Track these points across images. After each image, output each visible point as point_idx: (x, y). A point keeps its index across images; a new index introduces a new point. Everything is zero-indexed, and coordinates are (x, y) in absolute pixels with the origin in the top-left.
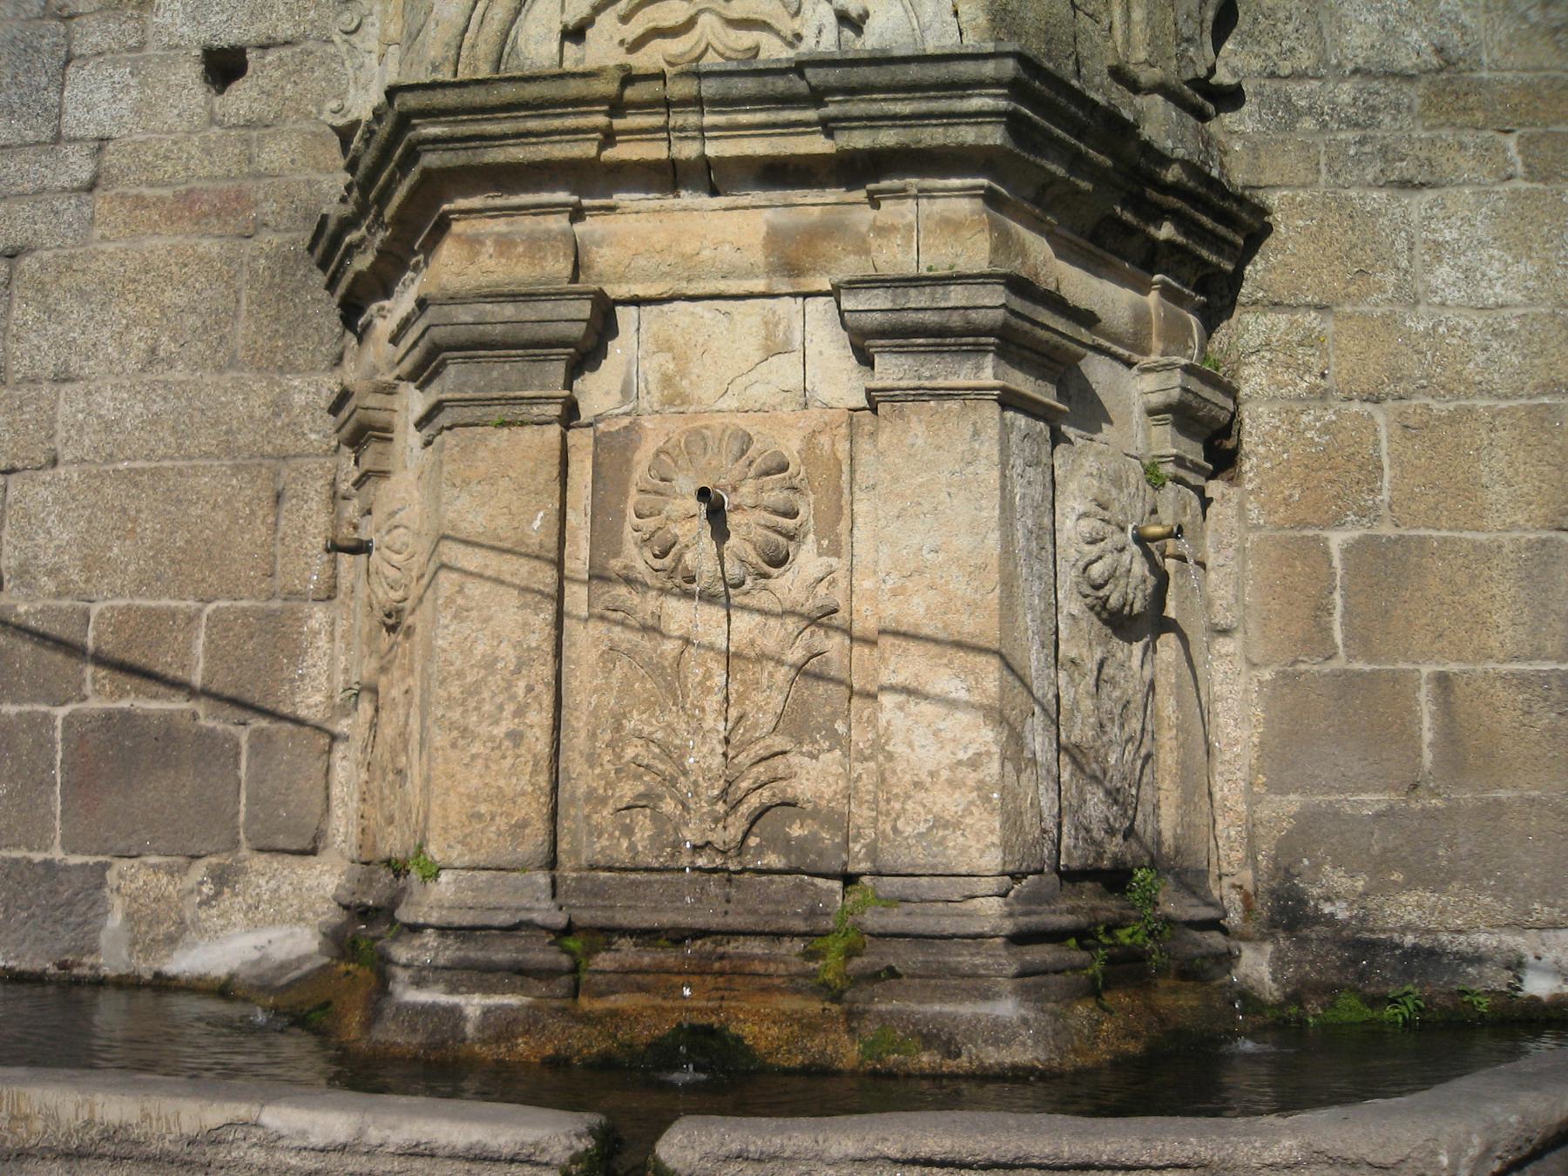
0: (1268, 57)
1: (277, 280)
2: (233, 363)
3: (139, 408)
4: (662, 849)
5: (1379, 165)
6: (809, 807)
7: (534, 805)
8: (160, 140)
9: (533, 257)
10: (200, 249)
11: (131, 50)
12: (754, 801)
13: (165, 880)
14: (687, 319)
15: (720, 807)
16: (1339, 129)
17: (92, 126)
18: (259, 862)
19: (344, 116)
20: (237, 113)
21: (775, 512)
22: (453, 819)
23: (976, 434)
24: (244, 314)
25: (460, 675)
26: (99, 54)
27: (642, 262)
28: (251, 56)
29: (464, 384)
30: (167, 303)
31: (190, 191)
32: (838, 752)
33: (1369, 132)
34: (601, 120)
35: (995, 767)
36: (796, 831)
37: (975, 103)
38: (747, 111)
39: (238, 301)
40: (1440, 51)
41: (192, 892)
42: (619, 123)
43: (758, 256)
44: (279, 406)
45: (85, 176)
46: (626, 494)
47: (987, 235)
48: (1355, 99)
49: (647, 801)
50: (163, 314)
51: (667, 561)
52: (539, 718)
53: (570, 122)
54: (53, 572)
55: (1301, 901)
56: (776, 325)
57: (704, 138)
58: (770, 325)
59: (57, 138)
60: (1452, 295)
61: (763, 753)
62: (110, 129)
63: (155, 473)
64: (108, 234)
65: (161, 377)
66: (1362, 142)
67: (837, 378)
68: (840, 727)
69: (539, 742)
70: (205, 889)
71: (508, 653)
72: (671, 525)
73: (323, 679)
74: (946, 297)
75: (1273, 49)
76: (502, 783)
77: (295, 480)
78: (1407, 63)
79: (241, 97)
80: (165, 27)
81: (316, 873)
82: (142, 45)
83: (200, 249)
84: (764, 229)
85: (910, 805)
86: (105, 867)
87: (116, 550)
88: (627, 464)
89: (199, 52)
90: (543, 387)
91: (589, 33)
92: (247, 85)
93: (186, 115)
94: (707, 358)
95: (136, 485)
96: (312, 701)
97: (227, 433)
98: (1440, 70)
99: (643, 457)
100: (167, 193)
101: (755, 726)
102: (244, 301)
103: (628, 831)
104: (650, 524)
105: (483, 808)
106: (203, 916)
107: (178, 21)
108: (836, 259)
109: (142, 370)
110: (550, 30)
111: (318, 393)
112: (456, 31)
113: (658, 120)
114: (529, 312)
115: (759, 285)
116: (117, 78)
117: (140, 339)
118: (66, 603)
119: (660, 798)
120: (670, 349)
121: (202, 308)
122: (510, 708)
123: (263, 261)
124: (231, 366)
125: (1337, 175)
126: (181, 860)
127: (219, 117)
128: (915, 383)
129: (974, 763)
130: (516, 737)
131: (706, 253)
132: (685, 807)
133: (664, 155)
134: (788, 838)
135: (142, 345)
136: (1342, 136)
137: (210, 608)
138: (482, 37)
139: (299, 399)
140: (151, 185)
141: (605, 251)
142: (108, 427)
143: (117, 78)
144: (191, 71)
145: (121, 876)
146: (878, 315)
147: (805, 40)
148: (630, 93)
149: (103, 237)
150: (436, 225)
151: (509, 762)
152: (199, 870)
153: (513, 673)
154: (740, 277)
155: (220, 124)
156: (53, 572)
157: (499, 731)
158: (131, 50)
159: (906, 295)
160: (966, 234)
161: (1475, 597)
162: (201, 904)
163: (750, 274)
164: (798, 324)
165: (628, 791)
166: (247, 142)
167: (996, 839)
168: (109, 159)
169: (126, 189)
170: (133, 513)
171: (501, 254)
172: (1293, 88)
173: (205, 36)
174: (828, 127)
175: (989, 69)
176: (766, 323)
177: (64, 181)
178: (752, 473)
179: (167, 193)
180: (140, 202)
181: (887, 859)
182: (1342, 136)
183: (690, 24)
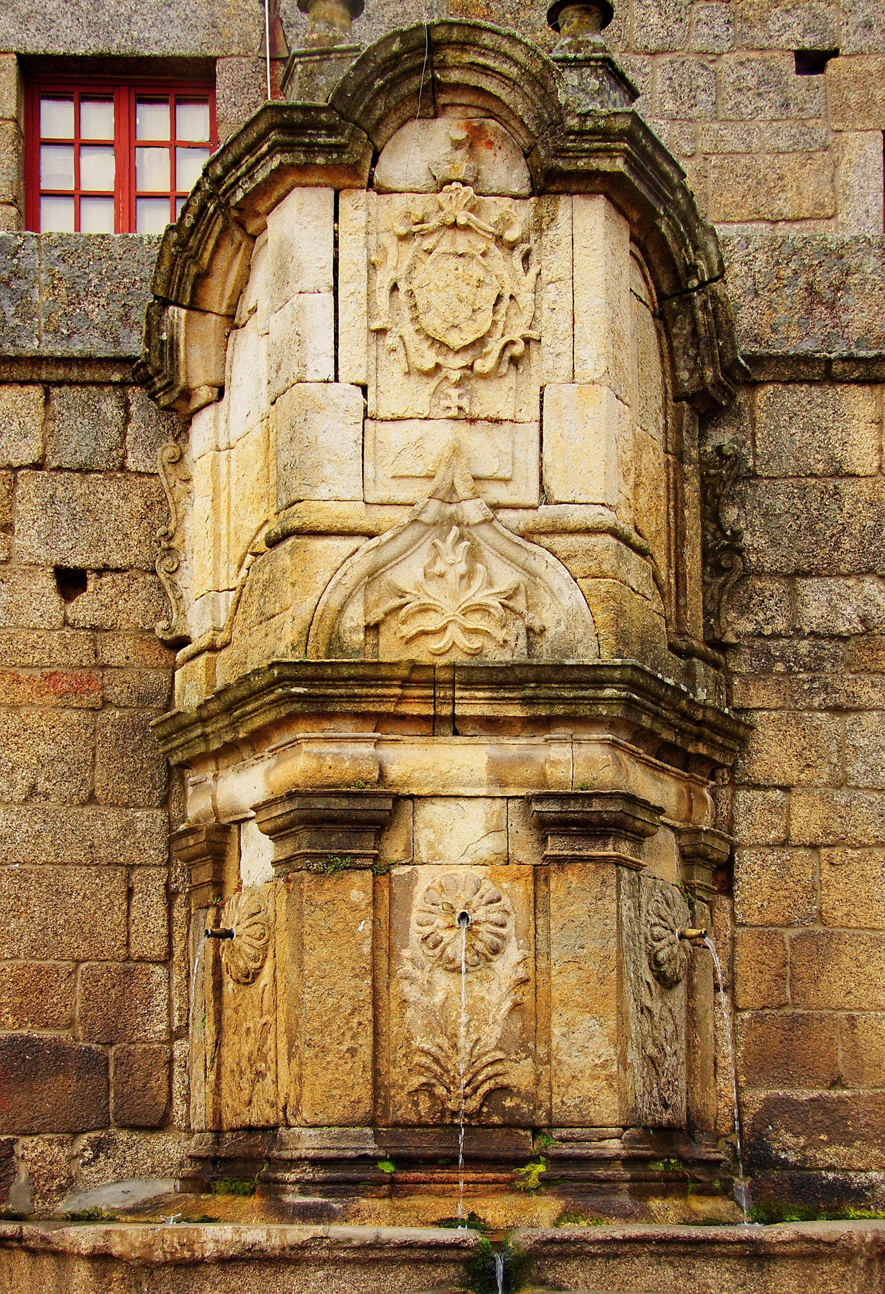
0: (758, 623)
1: (121, 742)
3: (25, 827)
4: (434, 1114)
5: (823, 696)
6: (515, 1090)
7: (364, 1090)
12: (486, 1087)
13: (56, 1150)
15: (468, 1090)
16: (799, 672)
18: (123, 1136)
19: (171, 633)
21: (496, 925)
22: (318, 1097)
23: (604, 882)
25: (320, 1015)
28: (91, 577)
29: (316, 844)
32: (530, 1060)
33: (817, 674)
35: (615, 1068)
36: (508, 1103)
37: (608, 692)
40: (863, 621)
41: (76, 1156)
42: (409, 692)
44: (128, 829)
46: (409, 911)
48: (809, 652)
49: (427, 1087)
51: (437, 951)
52: (366, 1041)
53: (380, 691)
55: (767, 1149)
61: (490, 1060)
66: (812, 681)
68: (531, 1045)
69: (365, 1053)
70: (86, 1154)
71: (347, 1005)
72: (438, 931)
73: (164, 1014)
74: (590, 806)
75: (761, 616)
76: (345, 1078)
77: (141, 881)
78: (843, 629)
79: (85, 608)
81: (163, 1142)
85: (570, 1089)
86: (12, 1143)
87: (13, 925)
88: (409, 895)
90: (361, 848)
91: (382, 629)
93: (46, 617)
94: (454, 834)
95: (26, 881)
96: (157, 1029)
97: (90, 847)
98: (862, 635)
100: (37, 673)
101: (485, 1045)
103: (416, 1104)
104: (427, 930)
105: (334, 1092)
106: (85, 1172)
111: (154, 822)
112: (307, 625)
113: (430, 692)
114: (358, 805)
115: (483, 792)
119: (434, 1085)
120: (432, 827)
122: (349, 1034)
125: (796, 703)
126: (67, 1136)
127: (71, 621)
128: (571, 853)
129: (604, 1066)
130: (352, 1051)
131: (454, 771)
132: (449, 1090)
133: (432, 713)
134: (504, 1107)
136: (800, 676)
144: (47, 583)
145: (24, 1148)
148: (416, 676)
151: (348, 1067)
152: (83, 1140)
153: (350, 1014)
154: (472, 786)
155: (72, 626)
157: (344, 1048)
159: (568, 803)
161: (869, 969)
162: (83, 1164)
165: (416, 1081)
166: (94, 641)
167: (616, 1107)
170: (24, 900)
172: (772, 644)
173: (56, 559)
174: (527, 701)
178: (483, 902)
181: (557, 1116)
182: (800, 676)
183: (444, 629)
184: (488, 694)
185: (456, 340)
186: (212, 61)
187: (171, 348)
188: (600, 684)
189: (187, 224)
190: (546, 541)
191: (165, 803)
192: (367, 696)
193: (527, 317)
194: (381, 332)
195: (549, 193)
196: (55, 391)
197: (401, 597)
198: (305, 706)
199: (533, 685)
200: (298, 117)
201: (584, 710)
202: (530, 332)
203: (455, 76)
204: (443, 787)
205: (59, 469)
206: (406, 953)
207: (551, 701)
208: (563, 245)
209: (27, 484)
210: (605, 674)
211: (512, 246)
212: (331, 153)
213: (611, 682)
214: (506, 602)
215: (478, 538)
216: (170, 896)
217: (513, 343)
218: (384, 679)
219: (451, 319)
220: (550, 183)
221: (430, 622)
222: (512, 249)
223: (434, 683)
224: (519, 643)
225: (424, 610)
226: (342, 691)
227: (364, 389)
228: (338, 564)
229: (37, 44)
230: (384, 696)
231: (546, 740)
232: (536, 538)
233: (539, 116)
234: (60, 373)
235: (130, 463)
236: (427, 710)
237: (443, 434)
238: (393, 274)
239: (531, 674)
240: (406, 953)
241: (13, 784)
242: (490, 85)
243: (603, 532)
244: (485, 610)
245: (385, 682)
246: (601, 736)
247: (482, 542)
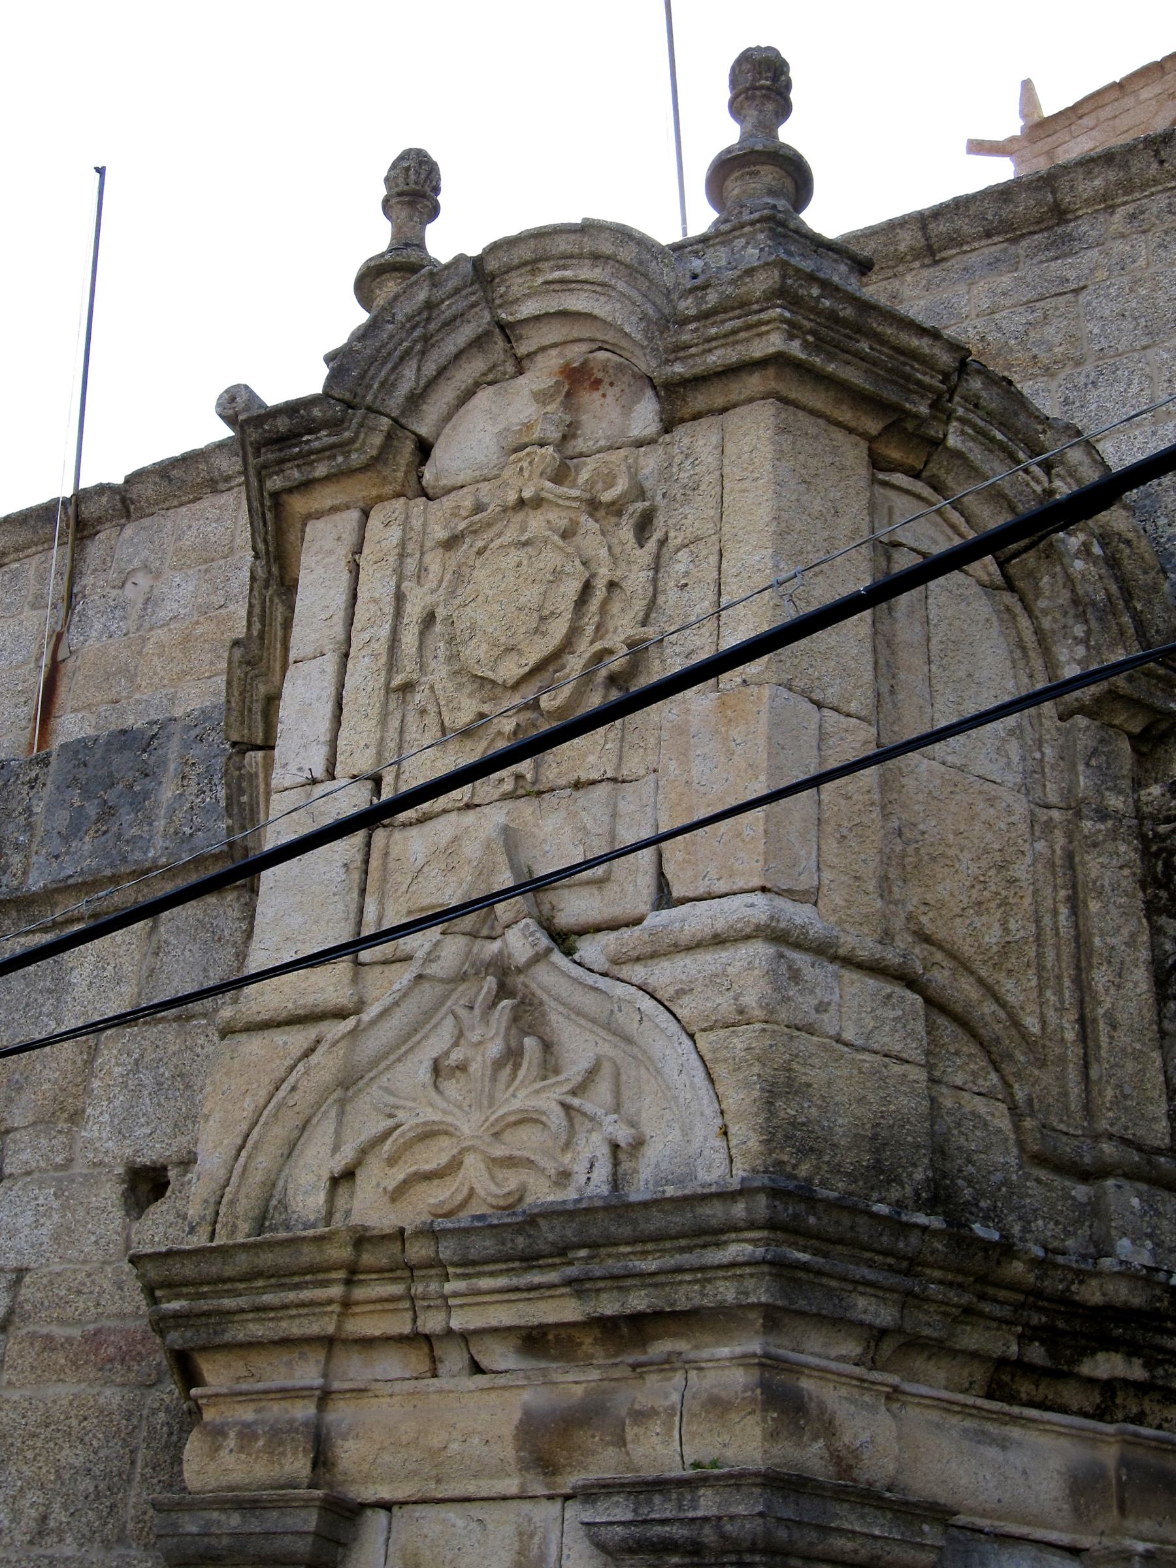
2: (121, 1540)
8: (75, 1271)
9: (271, 1453)
10: (102, 1400)
11: (58, 1167)
14: (438, 1528)
17: (12, 1255)
20: (152, 1240)
24: (138, 1478)
26: (28, 1173)
27: (386, 1457)
28: (172, 1174)
30: (63, 1463)
31: (98, 1332)
34: (336, 1291)
38: (492, 1274)
39: (133, 1463)
43: (508, 1451)
47: (757, 1417)
50: (59, 1477)
53: (306, 1295)
56: (531, 1536)
57: (449, 1307)
62: (29, 1260)
64: (14, 1379)
65: (49, 1552)
80: (91, 1141)
82: (70, 1161)
83: (102, 1400)
84: (517, 1415)
89: (120, 1170)
92: (165, 1207)
93: (103, 1242)
102: (139, 1464)
107: (104, 1135)
108: (594, 1453)
109: (31, 1542)
110: (319, 1178)
113: (397, 1289)
115: (511, 1486)
116: (41, 1201)
117: (32, 1505)
121: (96, 1471)
123: (162, 1414)
124: (119, 1540)
131: (455, 1446)
135: (33, 1513)
138: (243, 1191)
140: (62, 1322)
141: (350, 1444)
143: (41, 1201)
144: (110, 1193)
146: (618, 1529)
147: (575, 1177)
148: (367, 1259)
149: (9, 1383)
154: (491, 1477)
158: (58, 1167)
159: (649, 1502)
160: (734, 1416)
163: (501, 1471)
164: (554, 1536)
168: (24, 1292)
169: (36, 1328)
171: (241, 1449)
174: (578, 1286)
175: (739, 1210)
176: (521, 1534)
179: (76, 1332)
180: (49, 1343)
183: (455, 1165)
184: (502, 1282)
185: (510, 670)
187: (252, 810)
189: (255, 633)
190: (638, 973)
192: (285, 1307)
193: (639, 606)
194: (407, 688)
195: (682, 421)
197: (391, 1116)
198: (189, 1334)
199: (583, 1253)
201: (685, 1296)
202: (645, 629)
203: (528, 309)
204: (439, 1481)
207: (619, 1281)
208: (703, 487)
210: (714, 1213)
211: (616, 509)
212: (334, 457)
214: (569, 1100)
215: (539, 992)
217: (609, 652)
218: (312, 1269)
219: (503, 639)
221: (433, 1157)
222: (619, 514)
224: (594, 1175)
225: (428, 1134)
226: (242, 1302)
228: (281, 1073)
230: (312, 1304)
231: (634, 1367)
232: (625, 972)
233: (644, 317)
236: (401, 1325)
238: (429, 599)
239: (570, 1232)
241: (16, 1515)
242: (577, 302)
243: (748, 937)
244: (536, 1121)
245: (316, 1272)
246: (738, 1350)
247: (545, 997)
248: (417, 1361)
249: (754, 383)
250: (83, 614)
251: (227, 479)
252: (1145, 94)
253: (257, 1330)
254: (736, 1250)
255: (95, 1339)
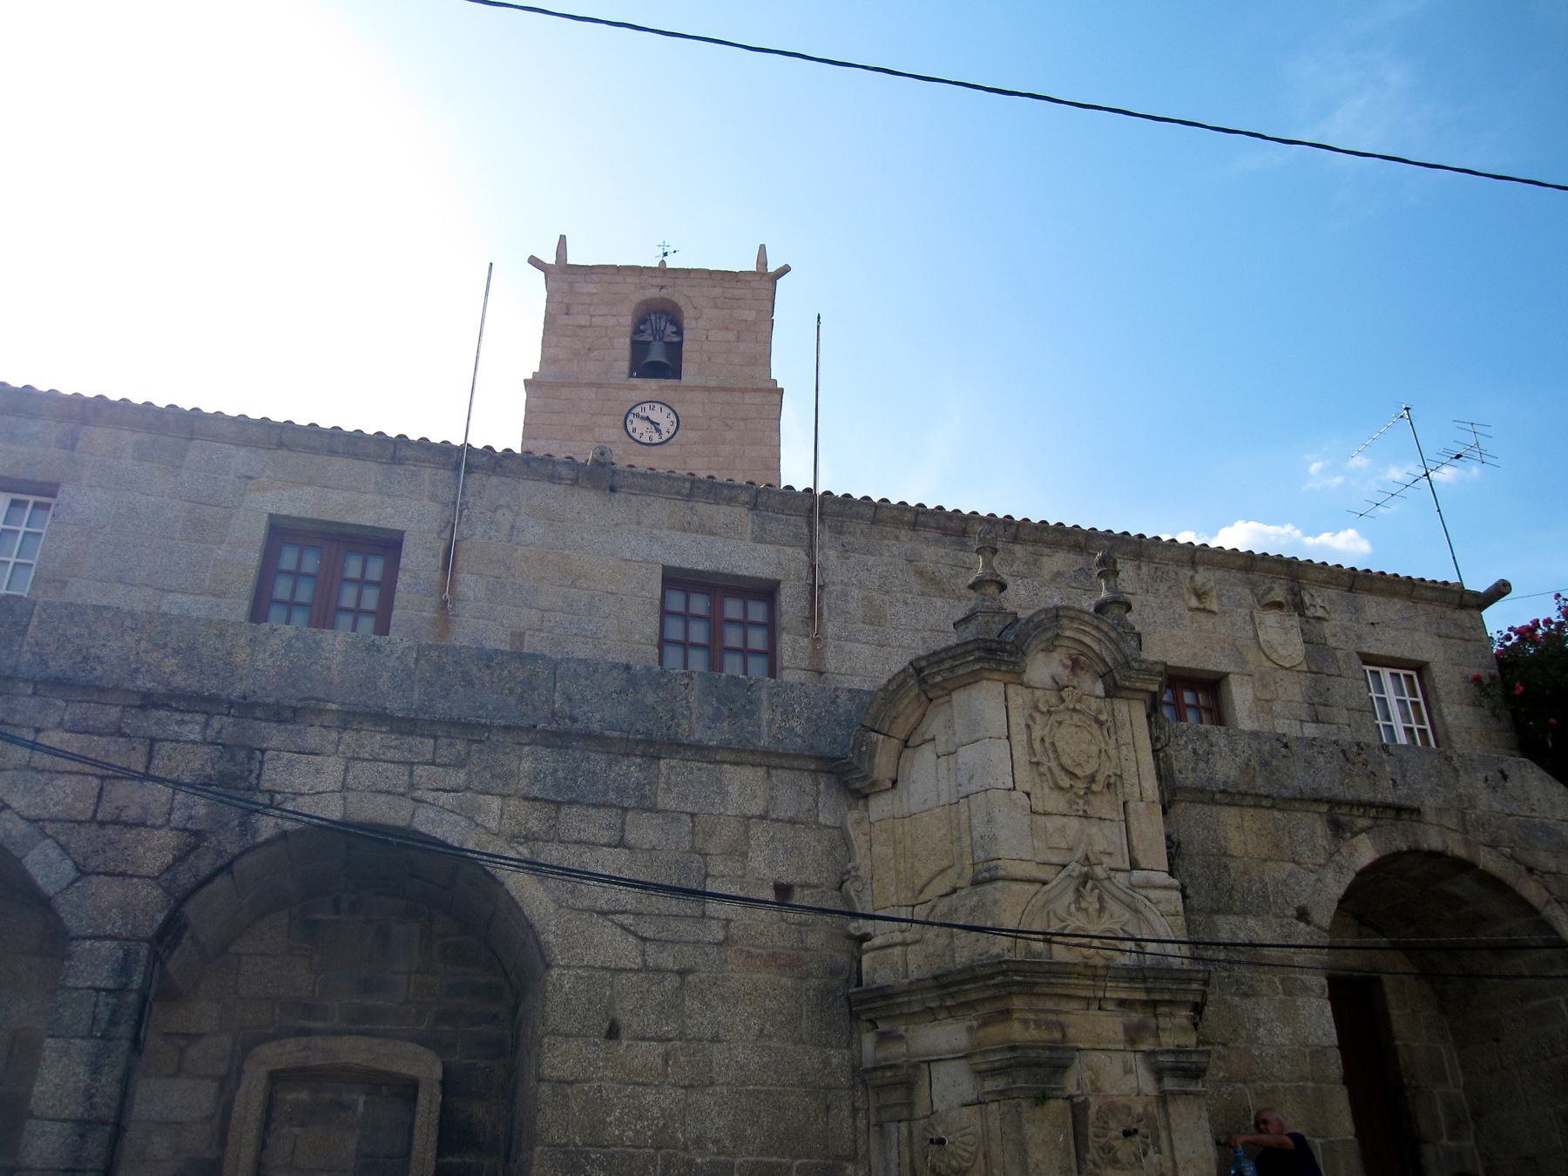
28: (797, 890)
43: (1121, 1036)
44: (826, 1063)
45: (721, 937)
54: (716, 1142)
58: (1125, 1062)
59: (704, 915)
60: (1266, 1040)
63: (768, 1093)
67: (1148, 1086)
99: (1093, 1110)
115: (1121, 1047)
118: (722, 1158)
137: (798, 1162)
139: (835, 1061)
142: (741, 1068)
150: (1001, 1012)
156: (716, 1142)
177: (709, 938)
186: (778, 583)
188: (1190, 981)
190: (1144, 892)
191: (848, 1047)
196: (774, 772)
200: (994, 646)
203: (1068, 633)
205: (778, 820)
206: (1089, 1156)
207: (1162, 990)
209: (757, 830)
210: (1193, 975)
213: (1196, 980)
216: (855, 1111)
220: (1113, 691)
223: (1094, 977)
227: (1028, 795)
229: (675, 561)
234: (776, 761)
235: (821, 819)
237: (1074, 824)
240: (1089, 1156)
248: (1083, 1004)
249: (1142, 695)
250: (469, 518)
251: (561, 479)
252: (629, 280)
253: (1046, 990)
254: (1195, 986)
255: (773, 955)
